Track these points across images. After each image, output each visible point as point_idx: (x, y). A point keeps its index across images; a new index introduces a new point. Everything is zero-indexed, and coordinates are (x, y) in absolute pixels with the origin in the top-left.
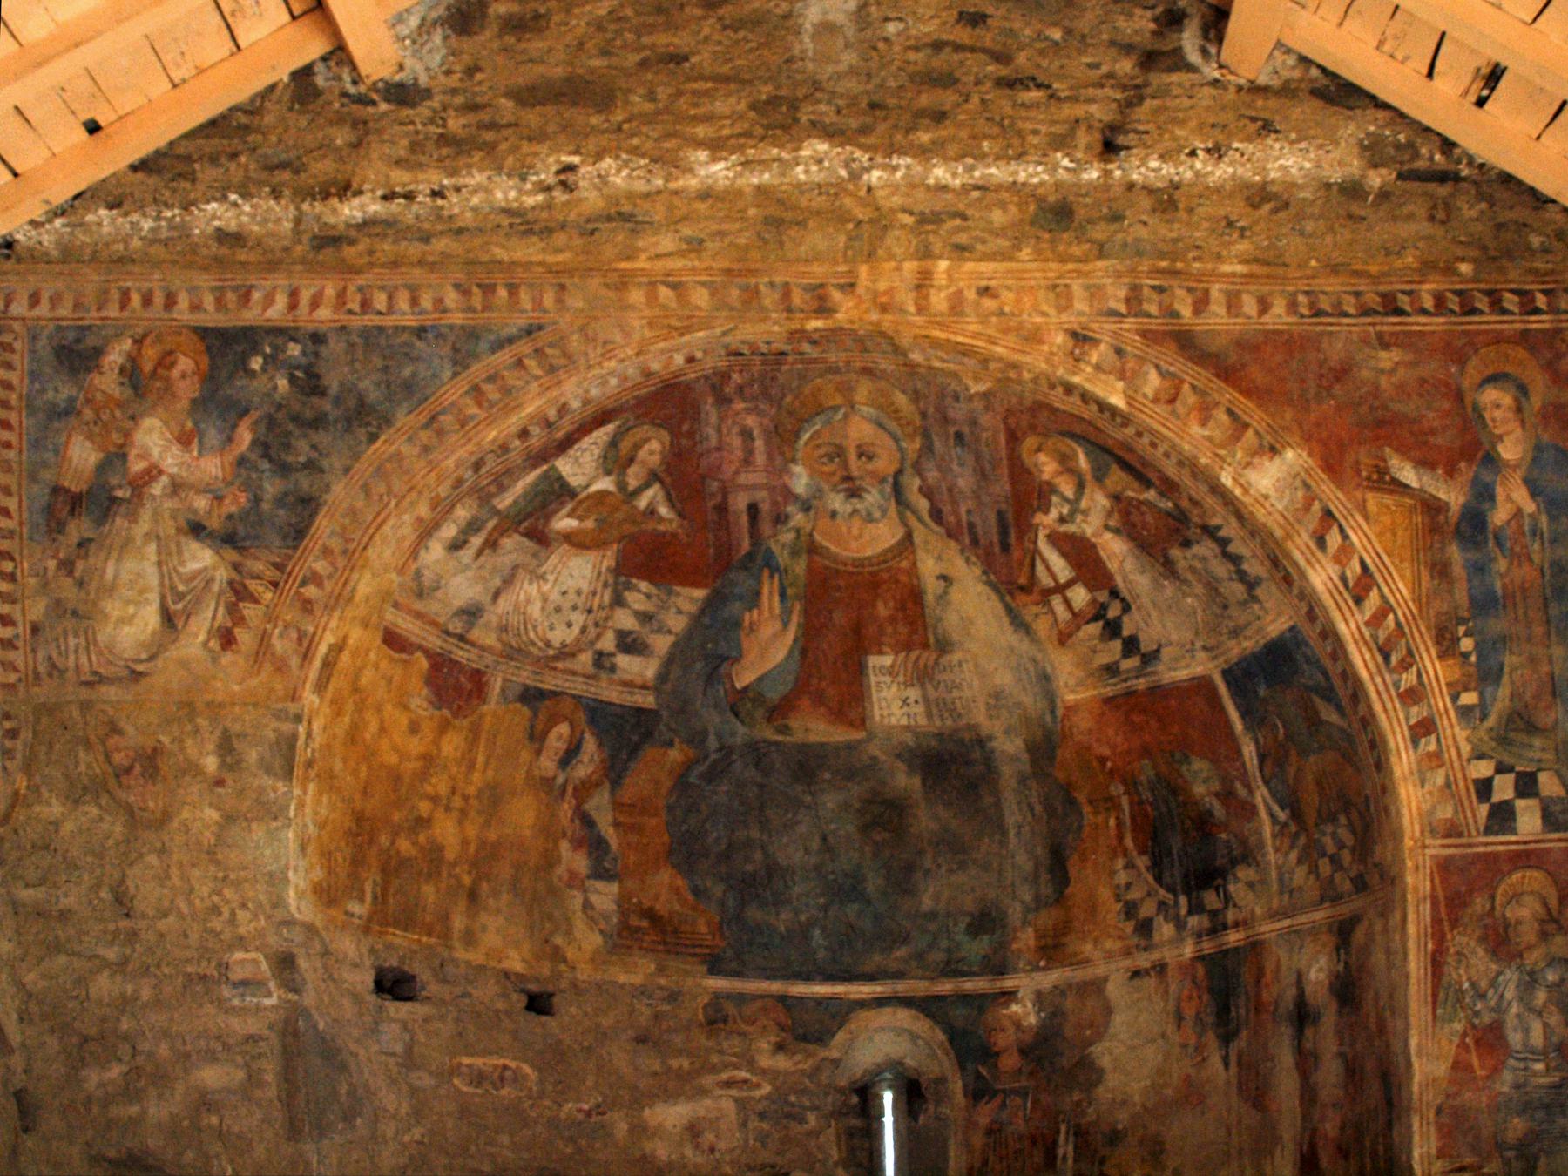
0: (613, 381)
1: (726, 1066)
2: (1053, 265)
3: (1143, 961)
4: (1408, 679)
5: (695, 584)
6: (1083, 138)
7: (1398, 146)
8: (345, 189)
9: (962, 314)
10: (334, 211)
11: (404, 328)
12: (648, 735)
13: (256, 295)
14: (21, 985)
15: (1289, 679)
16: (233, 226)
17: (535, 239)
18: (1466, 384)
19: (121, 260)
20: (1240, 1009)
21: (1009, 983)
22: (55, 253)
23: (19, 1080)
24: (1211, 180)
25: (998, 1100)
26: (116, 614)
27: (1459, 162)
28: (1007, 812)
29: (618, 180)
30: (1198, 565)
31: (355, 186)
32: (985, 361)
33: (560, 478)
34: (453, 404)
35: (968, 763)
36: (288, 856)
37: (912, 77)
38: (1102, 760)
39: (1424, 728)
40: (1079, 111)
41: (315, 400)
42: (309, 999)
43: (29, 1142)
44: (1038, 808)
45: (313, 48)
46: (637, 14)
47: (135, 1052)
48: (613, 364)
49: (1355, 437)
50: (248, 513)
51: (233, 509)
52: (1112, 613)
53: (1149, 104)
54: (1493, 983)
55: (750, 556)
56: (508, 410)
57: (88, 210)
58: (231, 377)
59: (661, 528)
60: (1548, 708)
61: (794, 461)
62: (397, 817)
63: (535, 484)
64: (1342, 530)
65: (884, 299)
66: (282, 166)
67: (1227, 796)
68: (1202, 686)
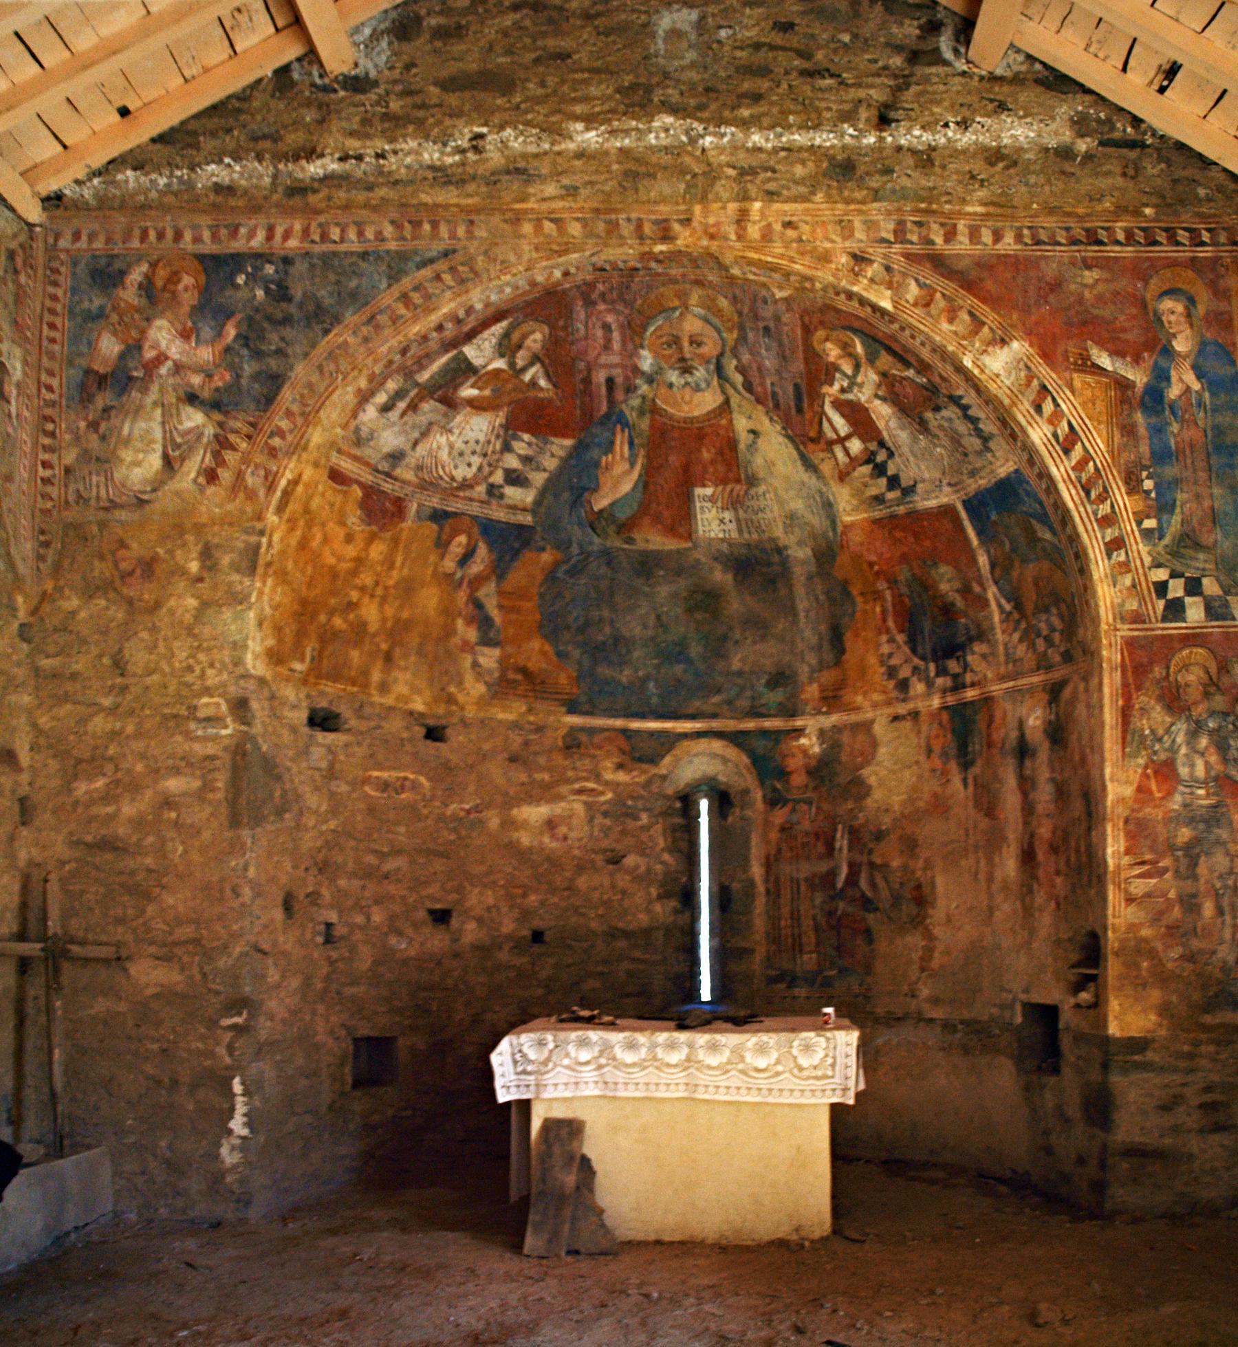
0: (508, 290)
1: (578, 779)
2: (840, 206)
3: (902, 709)
4: (1104, 509)
5: (564, 436)
6: (863, 114)
7: (1099, 121)
8: (312, 153)
9: (771, 241)
10: (303, 169)
11: (352, 253)
12: (526, 544)
13: (243, 231)
14: (34, 725)
15: (1015, 510)
16: (227, 181)
17: (452, 188)
18: (1148, 296)
19: (143, 207)
20: (976, 746)
21: (799, 723)
22: (93, 203)
23: (24, 790)
24: (959, 146)
25: (790, 805)
26: (129, 459)
27: (1145, 133)
28: (798, 602)
29: (516, 145)
30: (946, 424)
31: (319, 150)
32: (787, 275)
33: (466, 359)
34: (389, 306)
35: (769, 564)
36: (248, 633)
37: (737, 69)
38: (871, 565)
39: (1115, 545)
40: (861, 93)
41: (284, 305)
42: (257, 729)
43: (25, 832)
44: (822, 598)
45: (291, 51)
46: (535, 24)
47: (117, 770)
48: (508, 277)
49: (1062, 334)
50: (231, 386)
51: (220, 384)
52: (881, 457)
53: (914, 89)
54: (1168, 731)
55: (607, 416)
56: (429, 310)
57: (119, 171)
58: (222, 289)
59: (541, 395)
60: (1210, 532)
61: (642, 347)
62: (333, 601)
63: (447, 364)
64: (1054, 400)
65: (712, 230)
66: (265, 137)
67: (965, 591)
68: (947, 512)
